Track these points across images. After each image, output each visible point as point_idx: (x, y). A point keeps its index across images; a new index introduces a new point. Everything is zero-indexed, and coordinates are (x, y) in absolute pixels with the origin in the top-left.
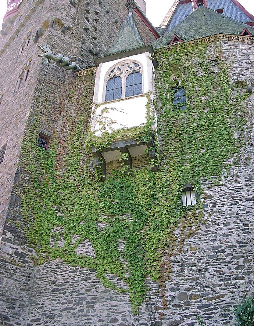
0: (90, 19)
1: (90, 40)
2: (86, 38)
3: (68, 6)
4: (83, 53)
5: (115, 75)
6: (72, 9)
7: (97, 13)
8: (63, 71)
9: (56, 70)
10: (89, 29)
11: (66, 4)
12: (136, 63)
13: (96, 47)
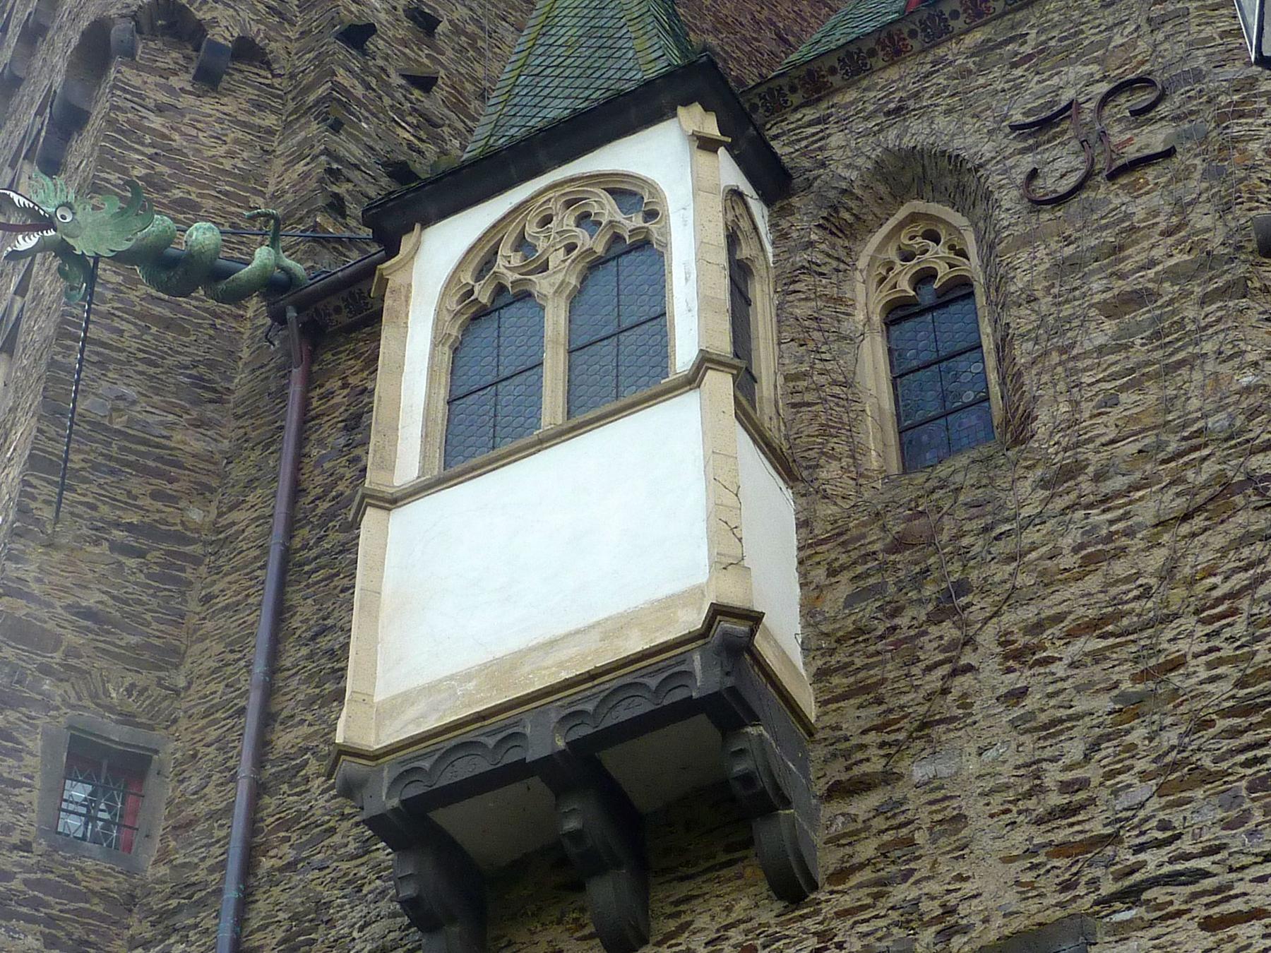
1: (387, 101)
2: (359, 91)
4: (341, 189)
5: (501, 289)
8: (218, 321)
9: (168, 324)
10: (370, 30)
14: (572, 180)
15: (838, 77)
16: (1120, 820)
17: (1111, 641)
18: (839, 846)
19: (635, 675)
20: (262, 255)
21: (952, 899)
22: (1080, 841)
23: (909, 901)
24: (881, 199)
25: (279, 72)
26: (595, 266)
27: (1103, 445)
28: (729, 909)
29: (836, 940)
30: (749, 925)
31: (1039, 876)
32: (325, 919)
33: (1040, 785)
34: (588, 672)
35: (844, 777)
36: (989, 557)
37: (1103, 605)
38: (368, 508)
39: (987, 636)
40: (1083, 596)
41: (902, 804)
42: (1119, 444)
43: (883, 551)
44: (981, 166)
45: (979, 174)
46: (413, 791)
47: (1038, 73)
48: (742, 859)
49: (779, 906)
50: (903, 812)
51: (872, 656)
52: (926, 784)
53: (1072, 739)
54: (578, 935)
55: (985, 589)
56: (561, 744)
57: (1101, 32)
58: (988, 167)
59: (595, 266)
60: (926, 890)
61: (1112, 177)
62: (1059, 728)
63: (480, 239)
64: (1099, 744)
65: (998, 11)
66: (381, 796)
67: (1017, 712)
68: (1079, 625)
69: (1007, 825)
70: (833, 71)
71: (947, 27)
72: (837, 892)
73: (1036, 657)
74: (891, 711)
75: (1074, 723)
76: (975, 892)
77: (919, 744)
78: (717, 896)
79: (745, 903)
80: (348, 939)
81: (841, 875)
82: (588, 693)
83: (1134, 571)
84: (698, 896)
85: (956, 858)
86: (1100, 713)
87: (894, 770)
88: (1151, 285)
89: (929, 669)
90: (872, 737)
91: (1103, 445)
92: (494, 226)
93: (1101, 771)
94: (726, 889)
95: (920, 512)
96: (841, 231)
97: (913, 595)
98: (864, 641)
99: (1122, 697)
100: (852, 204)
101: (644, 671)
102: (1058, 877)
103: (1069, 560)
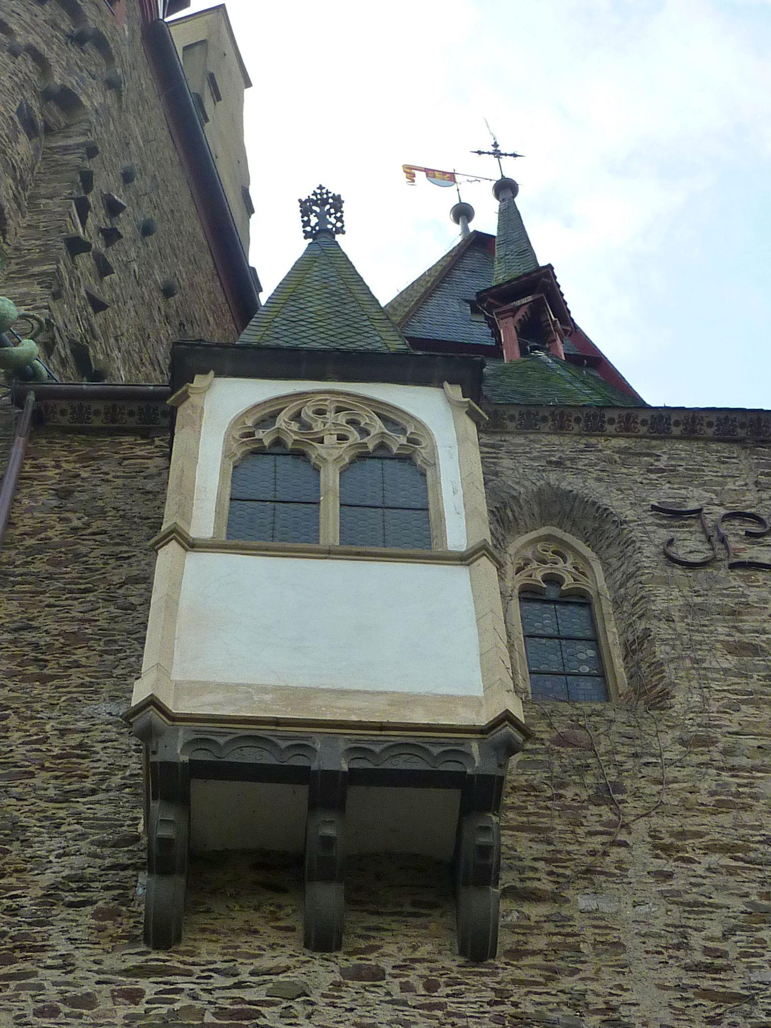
14: (348, 394)
15: (514, 424)
16: (753, 988)
17: (741, 864)
18: (513, 932)
19: (418, 739)
20: (28, 346)
21: (615, 1001)
22: (722, 993)
23: (576, 991)
24: (533, 515)
25: (8, 241)
26: (364, 457)
27: (729, 733)
28: (415, 948)
29: (511, 999)
30: (433, 965)
31: (688, 1006)
32: (22, 838)
33: (687, 944)
34: (381, 723)
35: (519, 885)
36: (640, 775)
37: (735, 837)
38: (173, 541)
39: (641, 827)
40: (718, 826)
41: (569, 920)
42: (741, 737)
43: (548, 740)
44: (625, 522)
45: (622, 527)
46: (201, 756)
47: (669, 482)
48: (427, 915)
49: (461, 960)
50: (571, 926)
51: (541, 808)
52: (589, 912)
53: (712, 920)
54: (272, 924)
55: (637, 795)
56: (345, 767)
57: (717, 476)
58: (631, 525)
59: (364, 457)
60: (591, 988)
61: (732, 566)
62: (700, 909)
63: (265, 402)
64: (735, 931)
65: (641, 433)
66: (176, 750)
67: (664, 887)
68: (716, 845)
69: (660, 963)
70: (512, 418)
71: (602, 427)
72: (512, 965)
73: (680, 855)
74: (560, 852)
75: (714, 910)
76: (635, 1002)
77: (583, 883)
78: (405, 935)
79: (429, 948)
80: (46, 860)
81: (517, 953)
82: (374, 738)
83: (757, 823)
84: (387, 930)
85: (618, 973)
86: (735, 910)
87: (562, 894)
88: (763, 645)
89: (591, 834)
90: (540, 865)
91: (729, 733)
92: (277, 399)
93: (739, 950)
94: (412, 932)
95: (580, 725)
96: (503, 523)
97: (576, 778)
98: (535, 796)
99: (751, 904)
100: (515, 508)
101: (426, 740)
102: (704, 1012)
103: (704, 798)
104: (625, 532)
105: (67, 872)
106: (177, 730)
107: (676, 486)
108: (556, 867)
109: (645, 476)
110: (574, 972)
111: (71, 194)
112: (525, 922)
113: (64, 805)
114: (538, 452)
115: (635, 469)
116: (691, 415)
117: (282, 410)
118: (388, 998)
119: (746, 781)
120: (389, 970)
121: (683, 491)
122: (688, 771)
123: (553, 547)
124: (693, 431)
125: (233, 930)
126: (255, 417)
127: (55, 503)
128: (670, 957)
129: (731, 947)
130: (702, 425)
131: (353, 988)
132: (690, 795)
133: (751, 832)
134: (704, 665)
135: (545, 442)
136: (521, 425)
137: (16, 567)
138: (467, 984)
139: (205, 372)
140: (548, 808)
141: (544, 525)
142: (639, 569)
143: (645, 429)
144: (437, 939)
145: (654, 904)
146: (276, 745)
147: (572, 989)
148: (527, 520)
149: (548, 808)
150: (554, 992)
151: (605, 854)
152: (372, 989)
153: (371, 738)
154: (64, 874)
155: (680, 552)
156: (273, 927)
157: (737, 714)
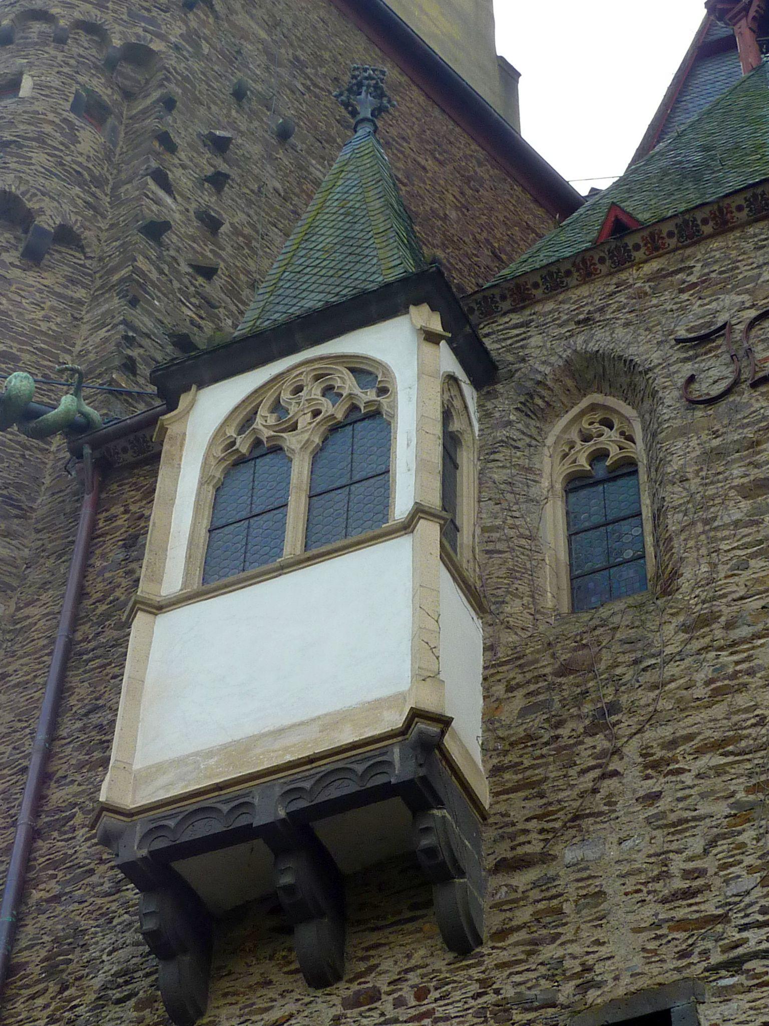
0: (176, 175)
1: (176, 284)
2: (154, 275)
3: (57, 121)
4: (134, 353)
5: (258, 443)
6: (81, 135)
7: (220, 145)
11: (51, 116)
12: (361, 366)
13: (214, 318)
14: (321, 358)
17: (731, 759)
18: (501, 910)
20: (67, 402)
27: (735, 600)
28: (409, 957)
32: (81, 943)
33: (666, 872)
34: (308, 756)
35: (509, 855)
38: (140, 615)
39: (632, 749)
40: (710, 721)
44: (650, 370)
47: (700, 298)
49: (450, 956)
50: (555, 887)
52: (574, 865)
53: (694, 835)
54: (286, 969)
55: (632, 710)
57: (752, 269)
61: (755, 385)
62: (685, 826)
63: (243, 401)
64: (716, 842)
67: (652, 811)
68: (706, 744)
71: (630, 256)
72: (498, 948)
74: (550, 804)
76: (609, 955)
78: (400, 945)
79: (422, 952)
81: (502, 934)
82: (307, 774)
83: (753, 703)
84: (385, 945)
85: (596, 926)
89: (583, 772)
90: (533, 825)
91: (735, 600)
93: (717, 863)
97: (574, 711)
99: (737, 805)
100: (544, 393)
101: (353, 759)
102: (676, 946)
103: (700, 691)
104: (650, 381)
105: (115, 969)
106: (135, 826)
107: (707, 300)
108: (547, 821)
109: (677, 300)
110: (554, 938)
111: (147, 169)
112: (513, 896)
113: (117, 896)
114: (567, 314)
115: (667, 295)
116: (716, 207)
117: (280, 393)
118: (383, 1019)
119: (745, 654)
120: (385, 988)
121: (714, 304)
122: (688, 661)
123: (598, 416)
124: (726, 222)
125: (250, 987)
126: (235, 424)
127: (121, 557)
128: (649, 893)
129: (709, 864)
130: (732, 212)
131: (351, 1018)
132: (684, 692)
133: (744, 716)
134: (716, 524)
135: (575, 298)
136: (547, 288)
137: (89, 642)
138: (455, 982)
139: (187, 389)
140: (543, 756)
141: (585, 395)
142: (660, 424)
143: (675, 240)
144: (429, 941)
145: (639, 835)
146: (220, 811)
147: (552, 958)
148: (563, 399)
149: (543, 756)
150: (534, 967)
151: (595, 791)
152: (368, 1014)
153: (304, 774)
154: (112, 972)
155: (705, 388)
156: (285, 973)
157: (745, 573)
